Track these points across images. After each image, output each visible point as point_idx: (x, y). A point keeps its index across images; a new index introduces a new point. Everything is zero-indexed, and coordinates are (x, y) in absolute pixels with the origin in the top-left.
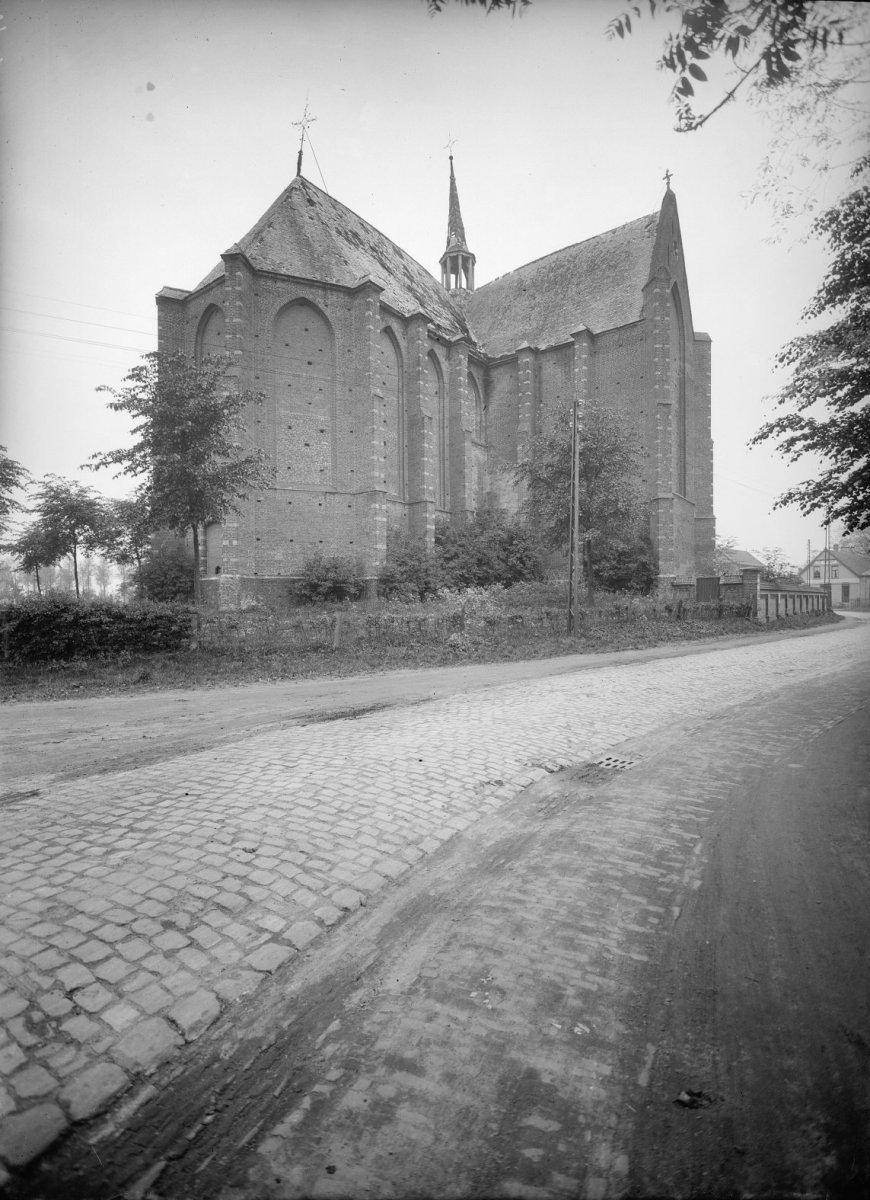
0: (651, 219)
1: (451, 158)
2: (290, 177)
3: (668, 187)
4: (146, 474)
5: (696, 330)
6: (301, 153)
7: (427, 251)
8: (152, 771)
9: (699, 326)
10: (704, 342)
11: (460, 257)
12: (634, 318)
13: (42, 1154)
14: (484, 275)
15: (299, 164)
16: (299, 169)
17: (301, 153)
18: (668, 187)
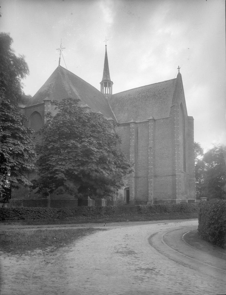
0: (174, 80)
1: (106, 46)
2: (58, 66)
3: (179, 72)
5: (188, 115)
6: (60, 58)
7: (94, 80)
8: (139, 132)
9: (189, 115)
10: (190, 120)
11: (108, 83)
13: (68, 224)
14: (116, 89)
16: (59, 63)
17: (60, 58)
18: (179, 72)
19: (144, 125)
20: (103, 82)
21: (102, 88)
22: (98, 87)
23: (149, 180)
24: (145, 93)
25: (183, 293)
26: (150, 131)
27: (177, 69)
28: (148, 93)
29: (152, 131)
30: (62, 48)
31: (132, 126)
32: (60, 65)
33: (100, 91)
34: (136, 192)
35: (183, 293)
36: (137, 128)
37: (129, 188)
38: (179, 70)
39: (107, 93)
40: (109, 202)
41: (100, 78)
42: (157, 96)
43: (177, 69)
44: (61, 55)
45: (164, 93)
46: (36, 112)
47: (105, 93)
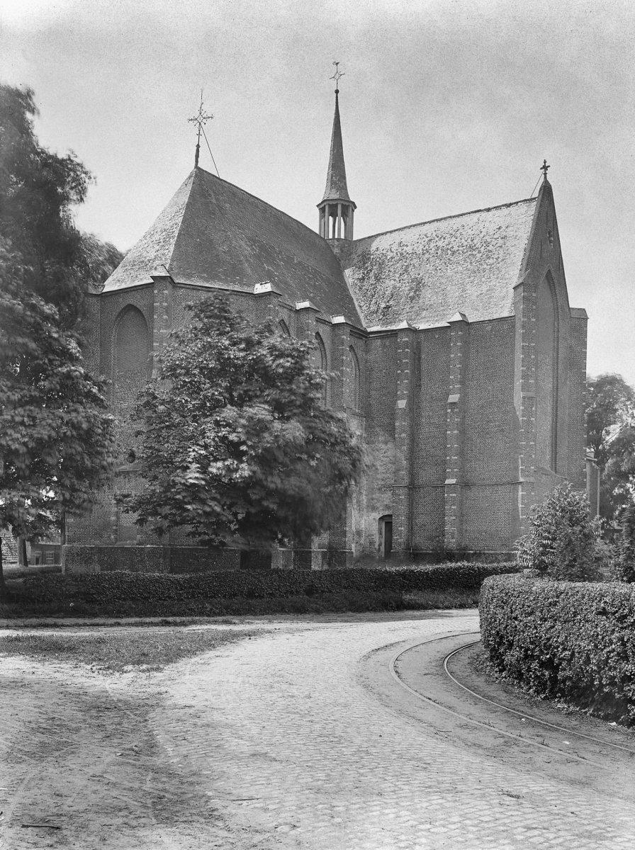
1: (337, 92)
3: (545, 177)
4: (166, 839)
6: (198, 146)
9: (576, 300)
10: (581, 319)
11: (339, 207)
12: (506, 314)
15: (197, 156)
16: (197, 162)
17: (198, 146)
18: (545, 177)
19: (437, 336)
20: (325, 203)
21: (324, 225)
22: (311, 220)
23: (446, 495)
24: (444, 238)
25: (242, 543)
26: (452, 356)
27: (541, 169)
28: (454, 239)
29: (459, 355)
30: (196, 122)
31: (403, 340)
32: (199, 165)
33: (317, 231)
34: (411, 529)
35: (242, 543)
36: (419, 343)
37: (390, 516)
38: (545, 174)
39: (336, 237)
40: (334, 553)
41: (319, 189)
42: (479, 252)
43: (541, 169)
44: (202, 138)
45: (501, 241)
46: (131, 308)
47: (331, 237)
